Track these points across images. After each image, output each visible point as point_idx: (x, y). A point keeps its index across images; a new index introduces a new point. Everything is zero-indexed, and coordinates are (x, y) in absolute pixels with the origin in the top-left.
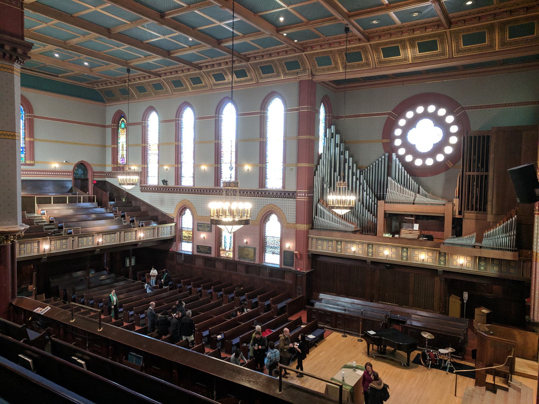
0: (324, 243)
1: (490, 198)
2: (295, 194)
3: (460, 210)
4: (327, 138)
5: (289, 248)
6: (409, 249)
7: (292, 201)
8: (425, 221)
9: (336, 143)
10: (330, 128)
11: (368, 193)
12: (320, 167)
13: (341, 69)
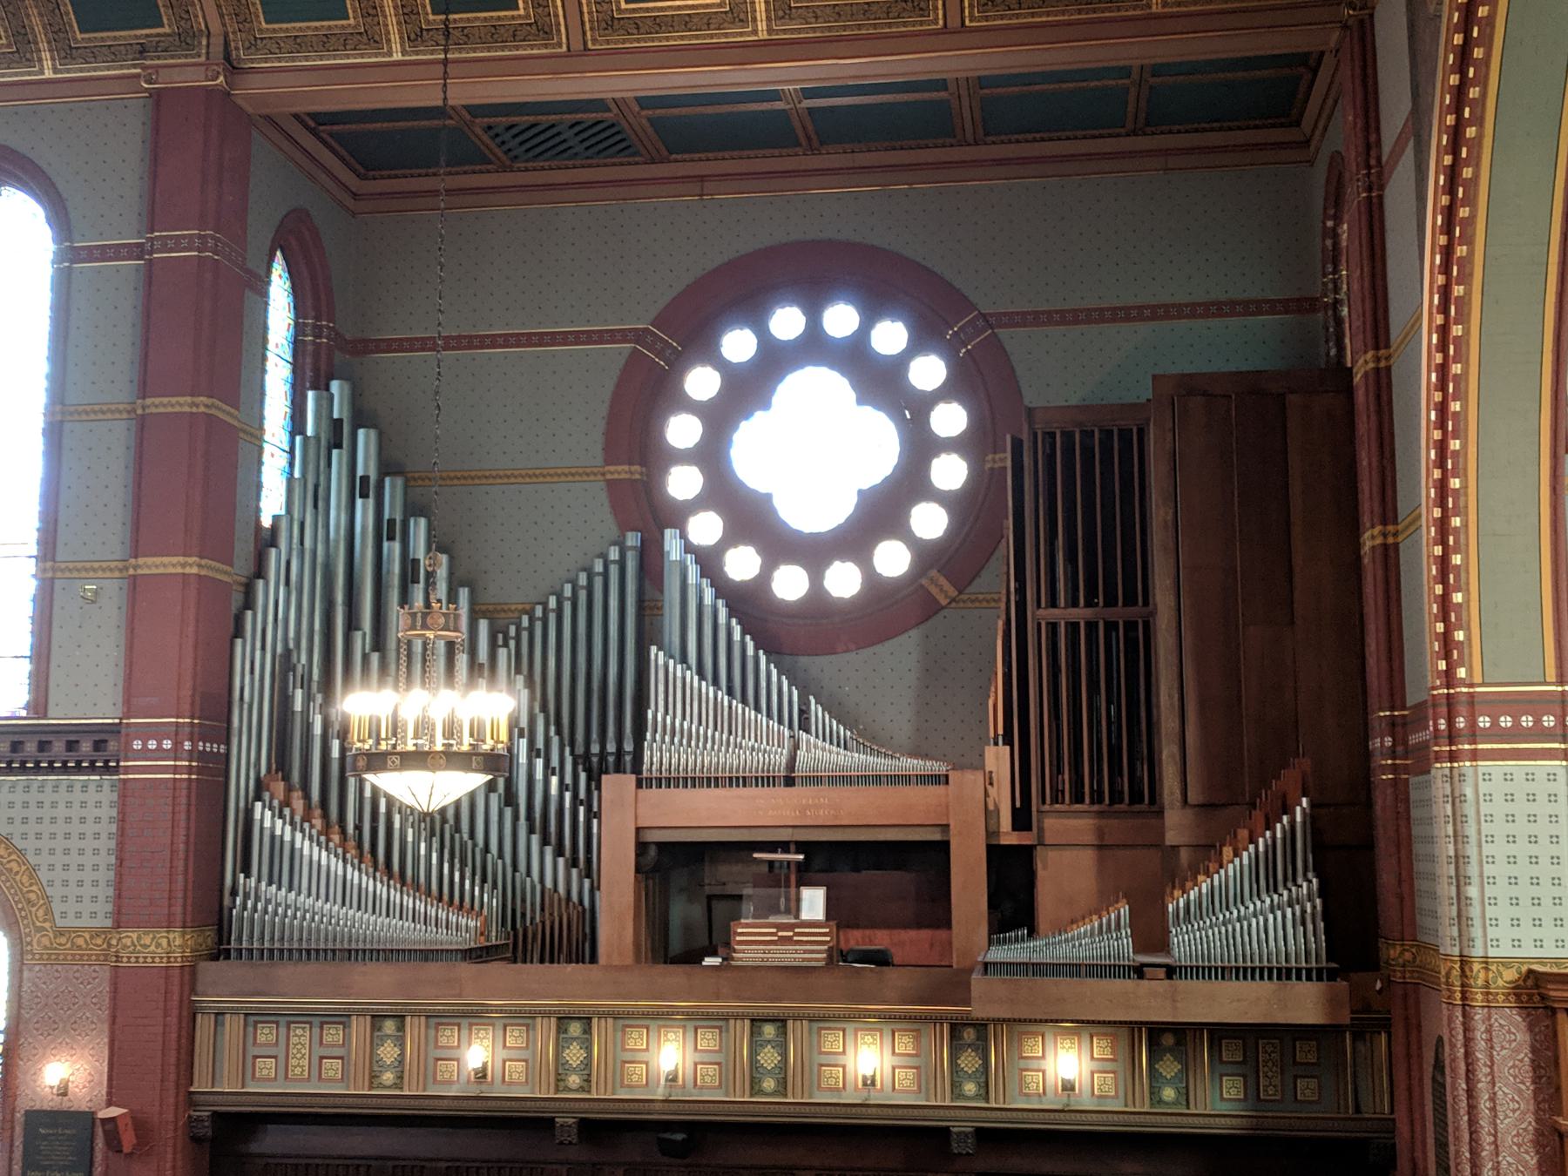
0: (294, 1040)
1: (1168, 722)
2: (112, 746)
3: (1018, 804)
4: (306, 439)
5: (63, 1091)
6: (790, 1023)
7: (92, 788)
8: (848, 877)
9: (360, 472)
10: (321, 385)
11: (540, 744)
12: (270, 592)
13: (396, 47)
